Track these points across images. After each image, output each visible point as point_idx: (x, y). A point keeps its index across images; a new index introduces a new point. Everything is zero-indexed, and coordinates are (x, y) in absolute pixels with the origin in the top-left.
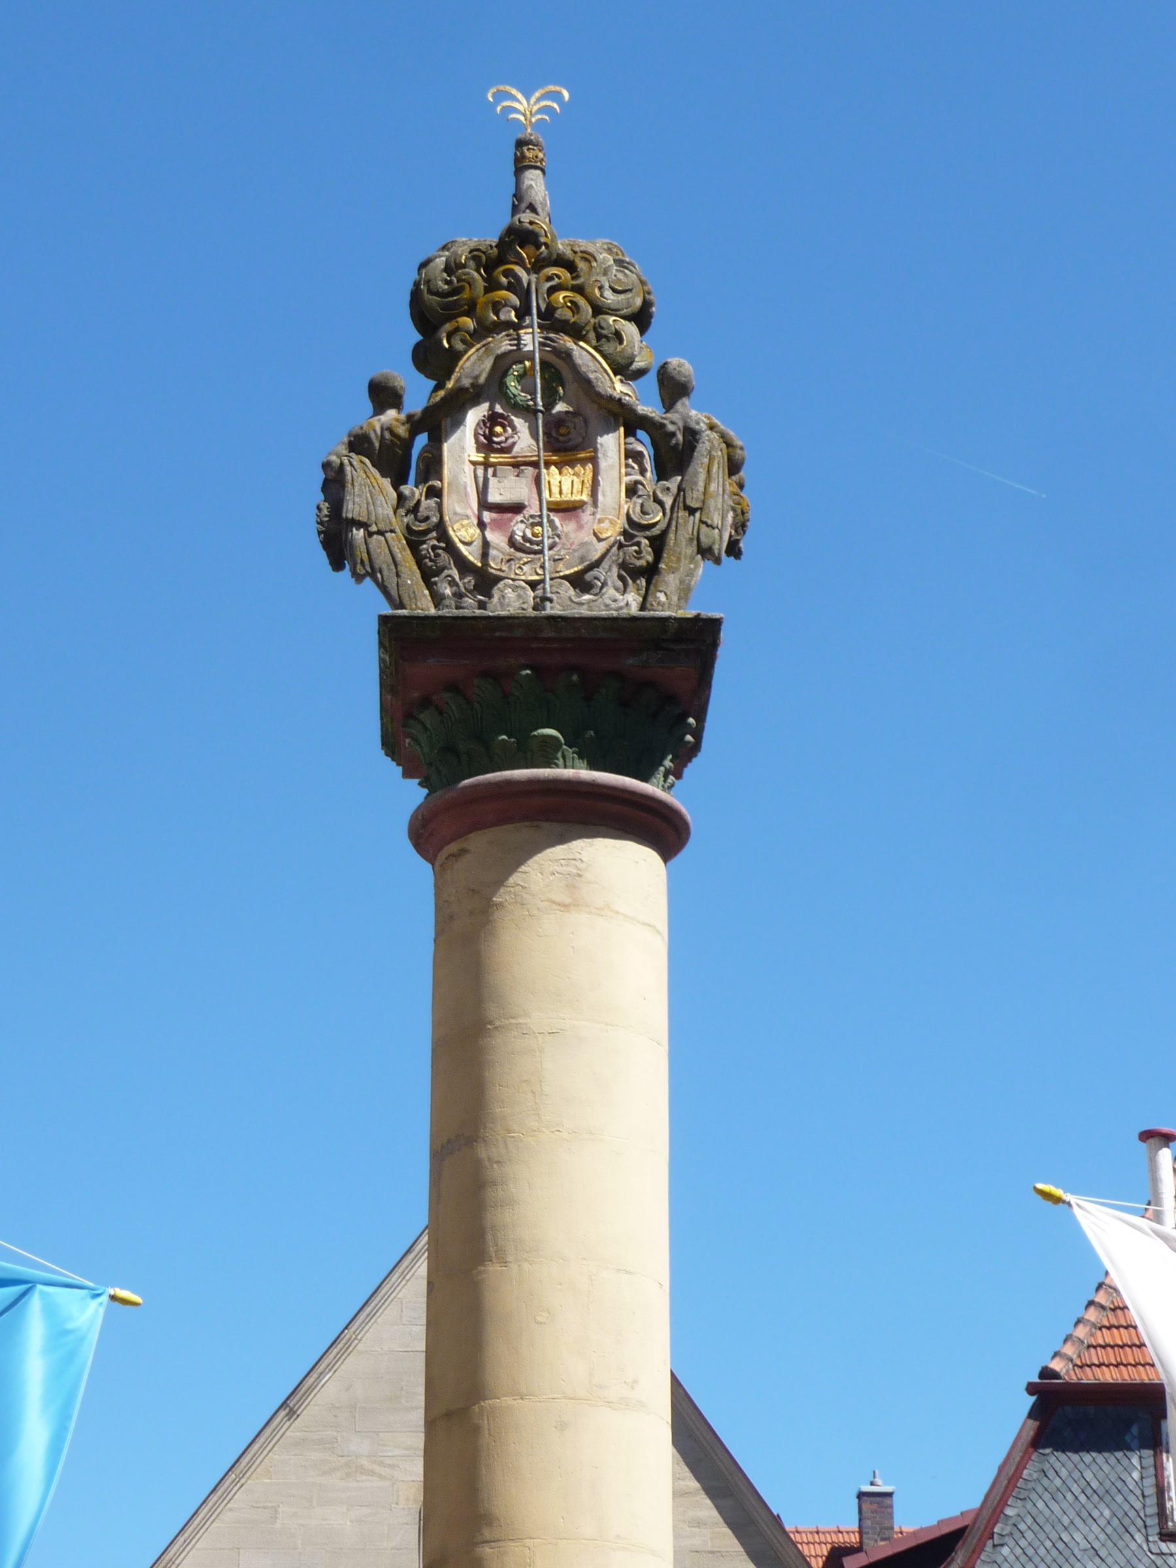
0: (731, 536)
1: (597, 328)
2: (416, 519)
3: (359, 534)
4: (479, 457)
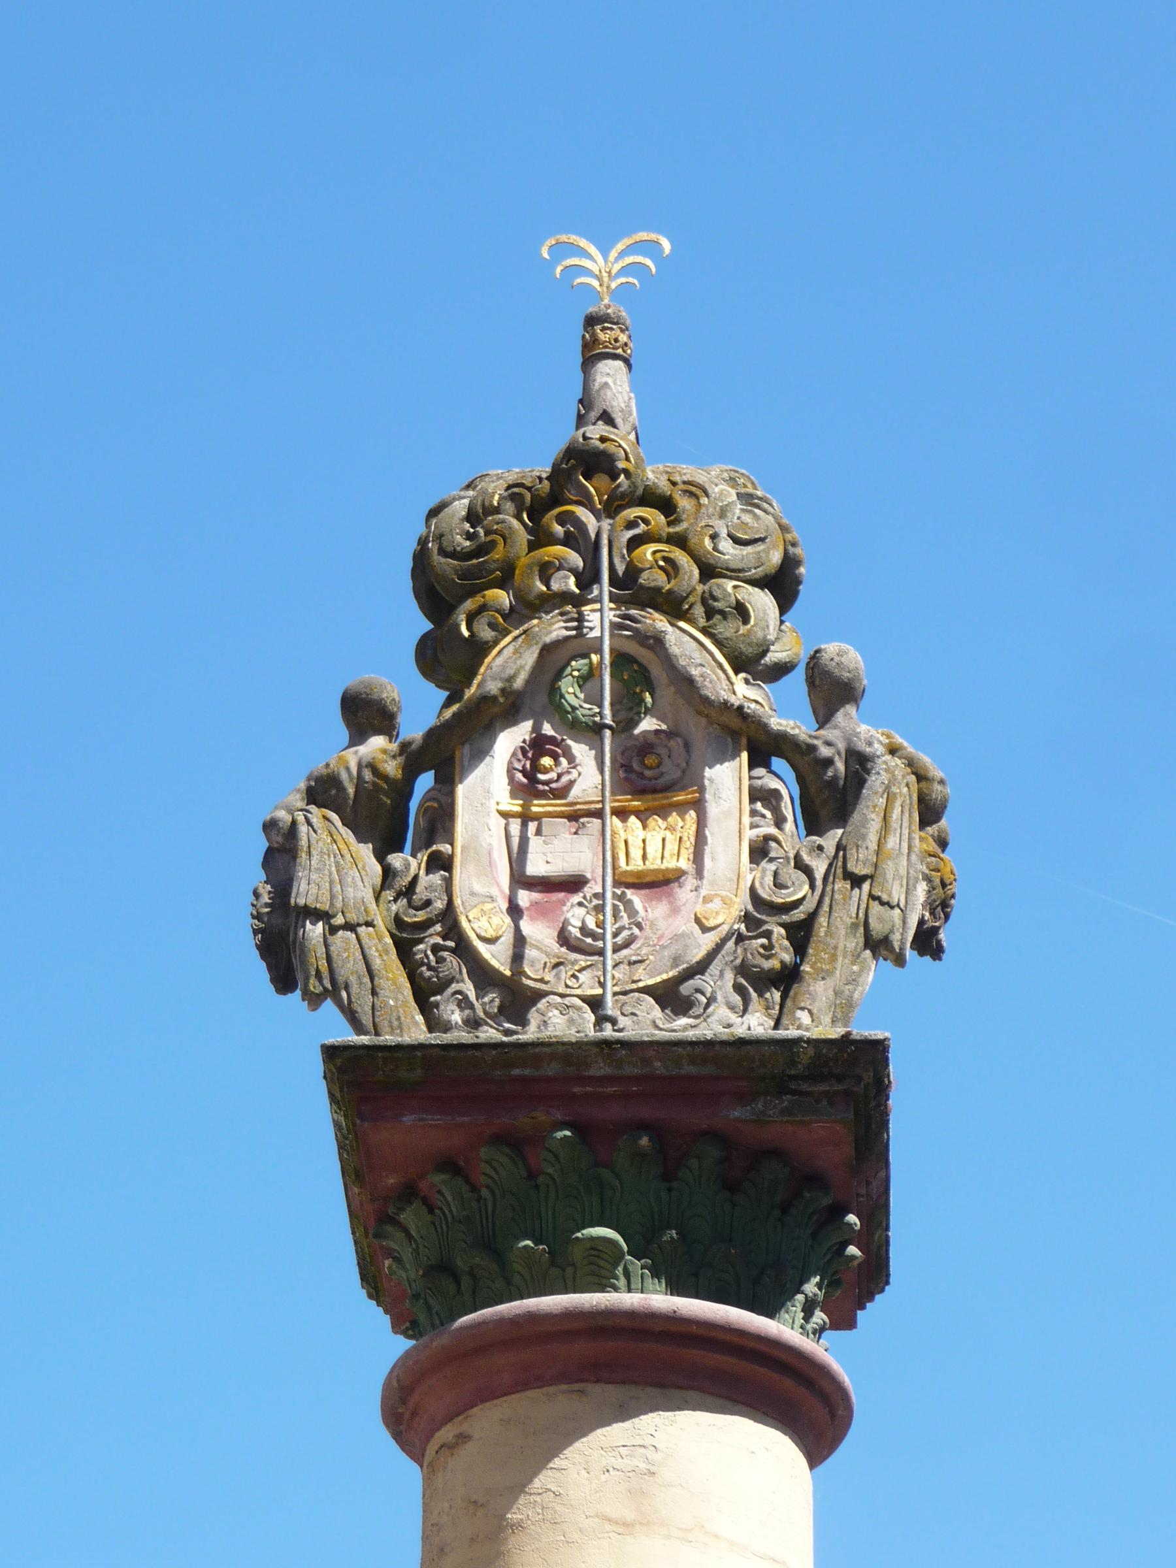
0: (921, 922)
1: (707, 601)
2: (410, 905)
3: (315, 931)
4: (515, 806)
